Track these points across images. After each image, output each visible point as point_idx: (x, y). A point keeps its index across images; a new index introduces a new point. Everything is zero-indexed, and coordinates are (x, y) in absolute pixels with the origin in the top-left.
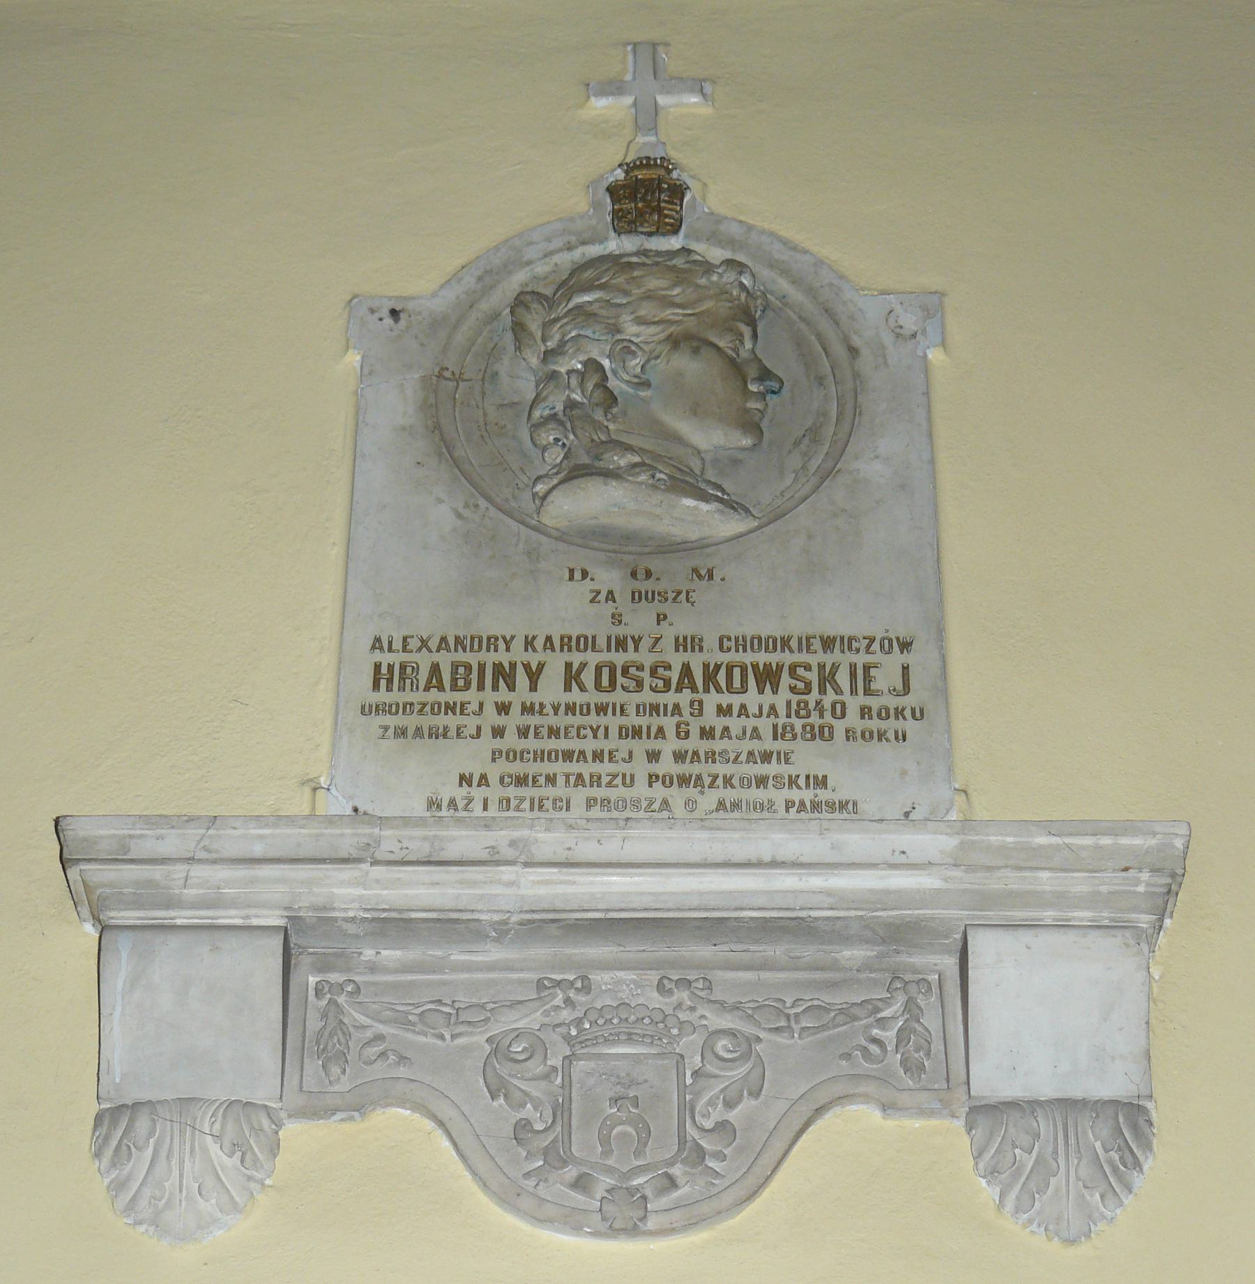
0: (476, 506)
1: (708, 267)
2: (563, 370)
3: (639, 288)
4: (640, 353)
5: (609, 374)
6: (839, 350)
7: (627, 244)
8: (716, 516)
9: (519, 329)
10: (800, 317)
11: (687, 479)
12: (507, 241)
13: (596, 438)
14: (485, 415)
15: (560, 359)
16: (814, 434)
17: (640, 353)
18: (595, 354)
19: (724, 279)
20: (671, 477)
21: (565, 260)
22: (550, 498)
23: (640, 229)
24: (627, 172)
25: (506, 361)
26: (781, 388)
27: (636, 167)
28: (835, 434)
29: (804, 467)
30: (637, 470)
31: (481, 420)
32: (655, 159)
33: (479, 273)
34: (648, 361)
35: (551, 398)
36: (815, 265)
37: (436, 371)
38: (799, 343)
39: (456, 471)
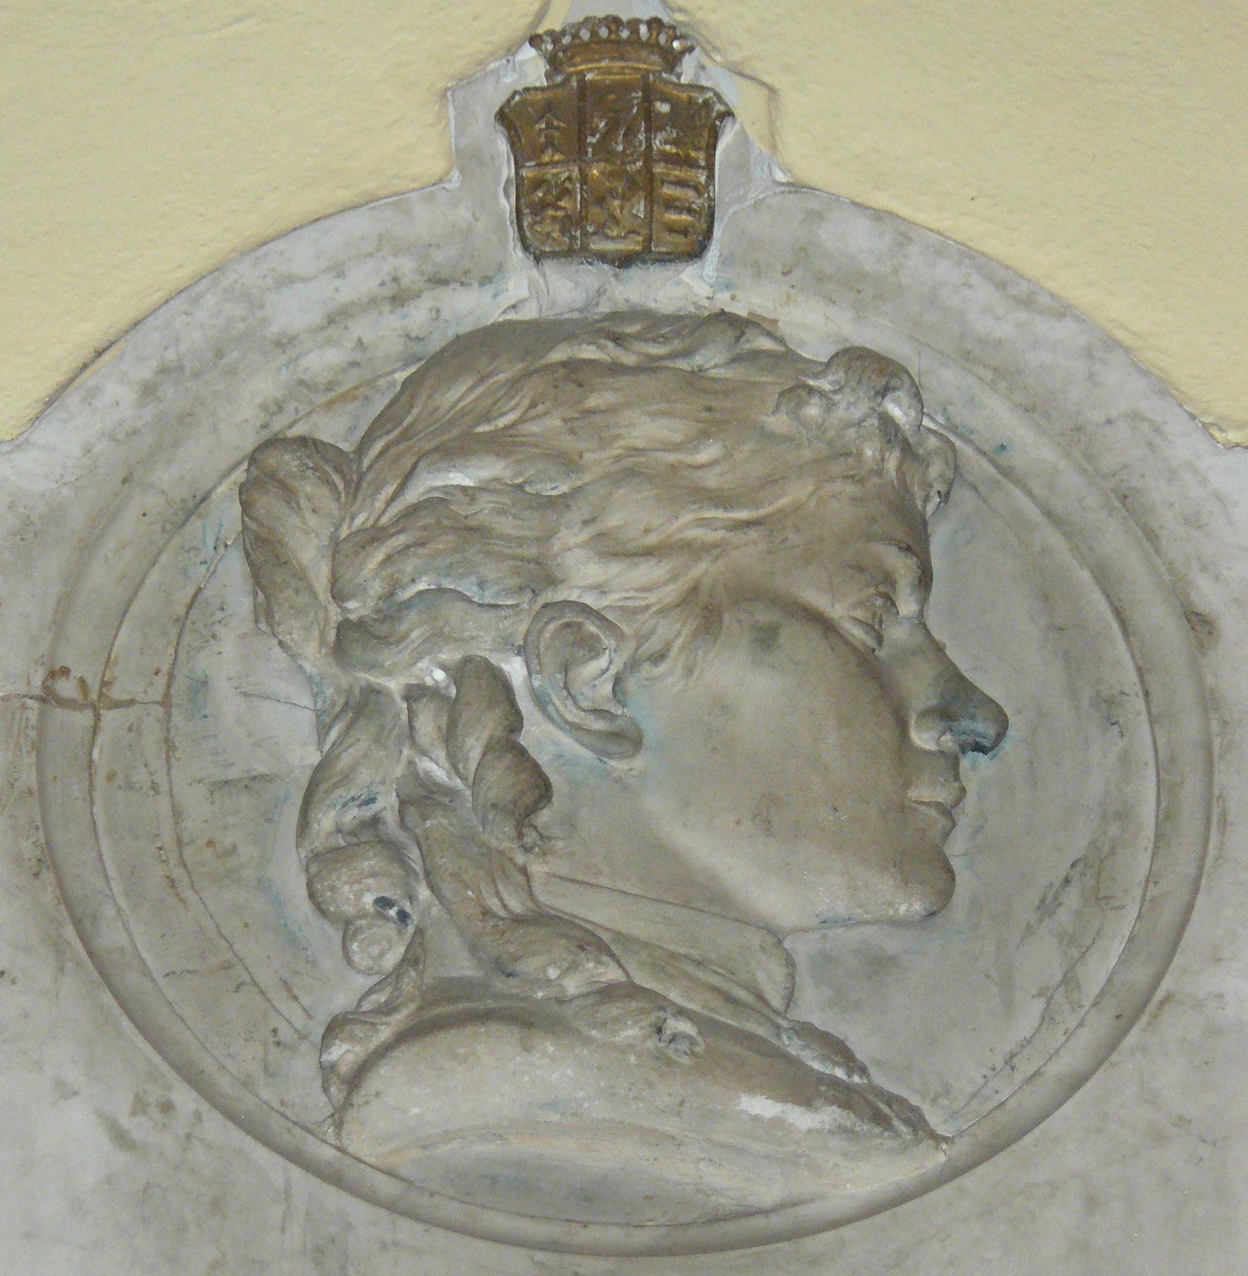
0: (167, 1107)
1: (791, 372)
2: (394, 685)
3: (603, 444)
4: (608, 642)
5: (525, 704)
6: (1158, 618)
7: (564, 289)
8: (835, 1142)
9: (265, 555)
10: (1048, 513)
11: (752, 1026)
12: (219, 269)
13: (494, 904)
14: (177, 814)
15: (388, 657)
16: (1093, 873)
17: (608, 642)
18: (483, 649)
19: (840, 413)
20: (707, 1026)
21: (385, 333)
22: (373, 1083)
23: (598, 245)
24: (554, 63)
25: (229, 644)
26: (1000, 736)
27: (578, 48)
28: (1152, 878)
29: (1069, 981)
30: (614, 1010)
31: (167, 828)
32: (634, 24)
33: (144, 373)
34: (633, 665)
35: (364, 776)
36: (1088, 353)
37: (37, 680)
38: (1048, 593)
39: (107, 998)
